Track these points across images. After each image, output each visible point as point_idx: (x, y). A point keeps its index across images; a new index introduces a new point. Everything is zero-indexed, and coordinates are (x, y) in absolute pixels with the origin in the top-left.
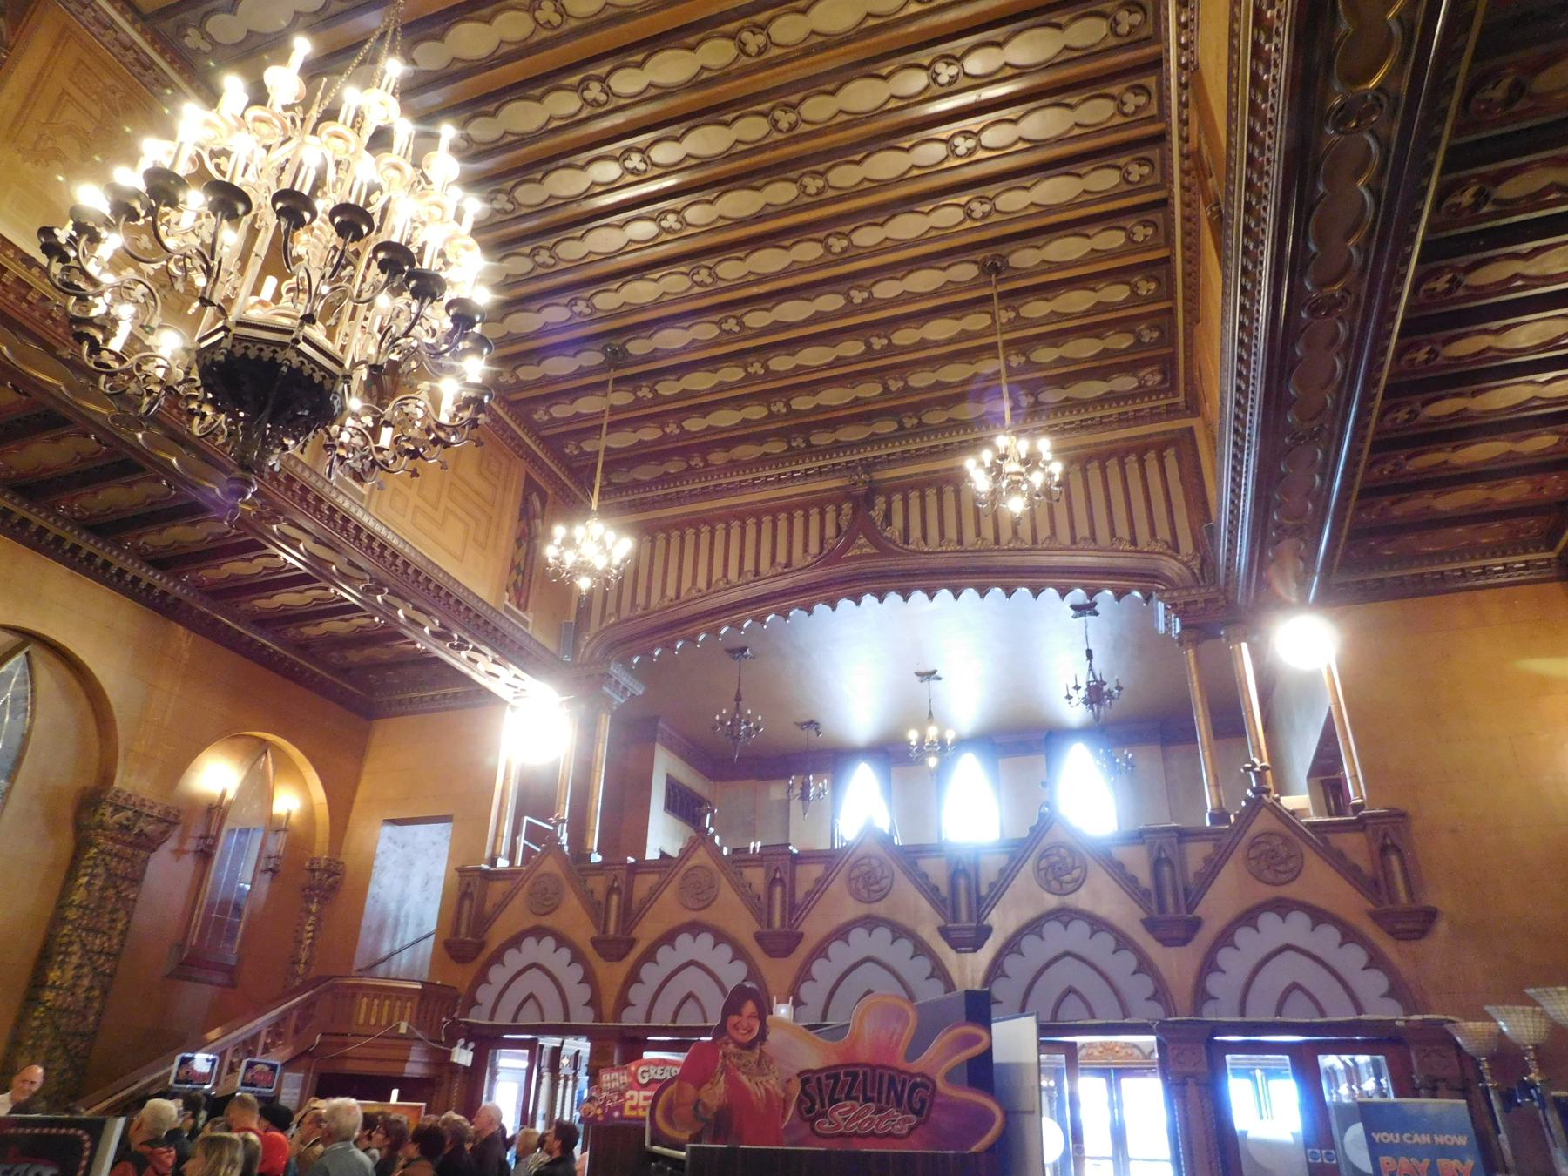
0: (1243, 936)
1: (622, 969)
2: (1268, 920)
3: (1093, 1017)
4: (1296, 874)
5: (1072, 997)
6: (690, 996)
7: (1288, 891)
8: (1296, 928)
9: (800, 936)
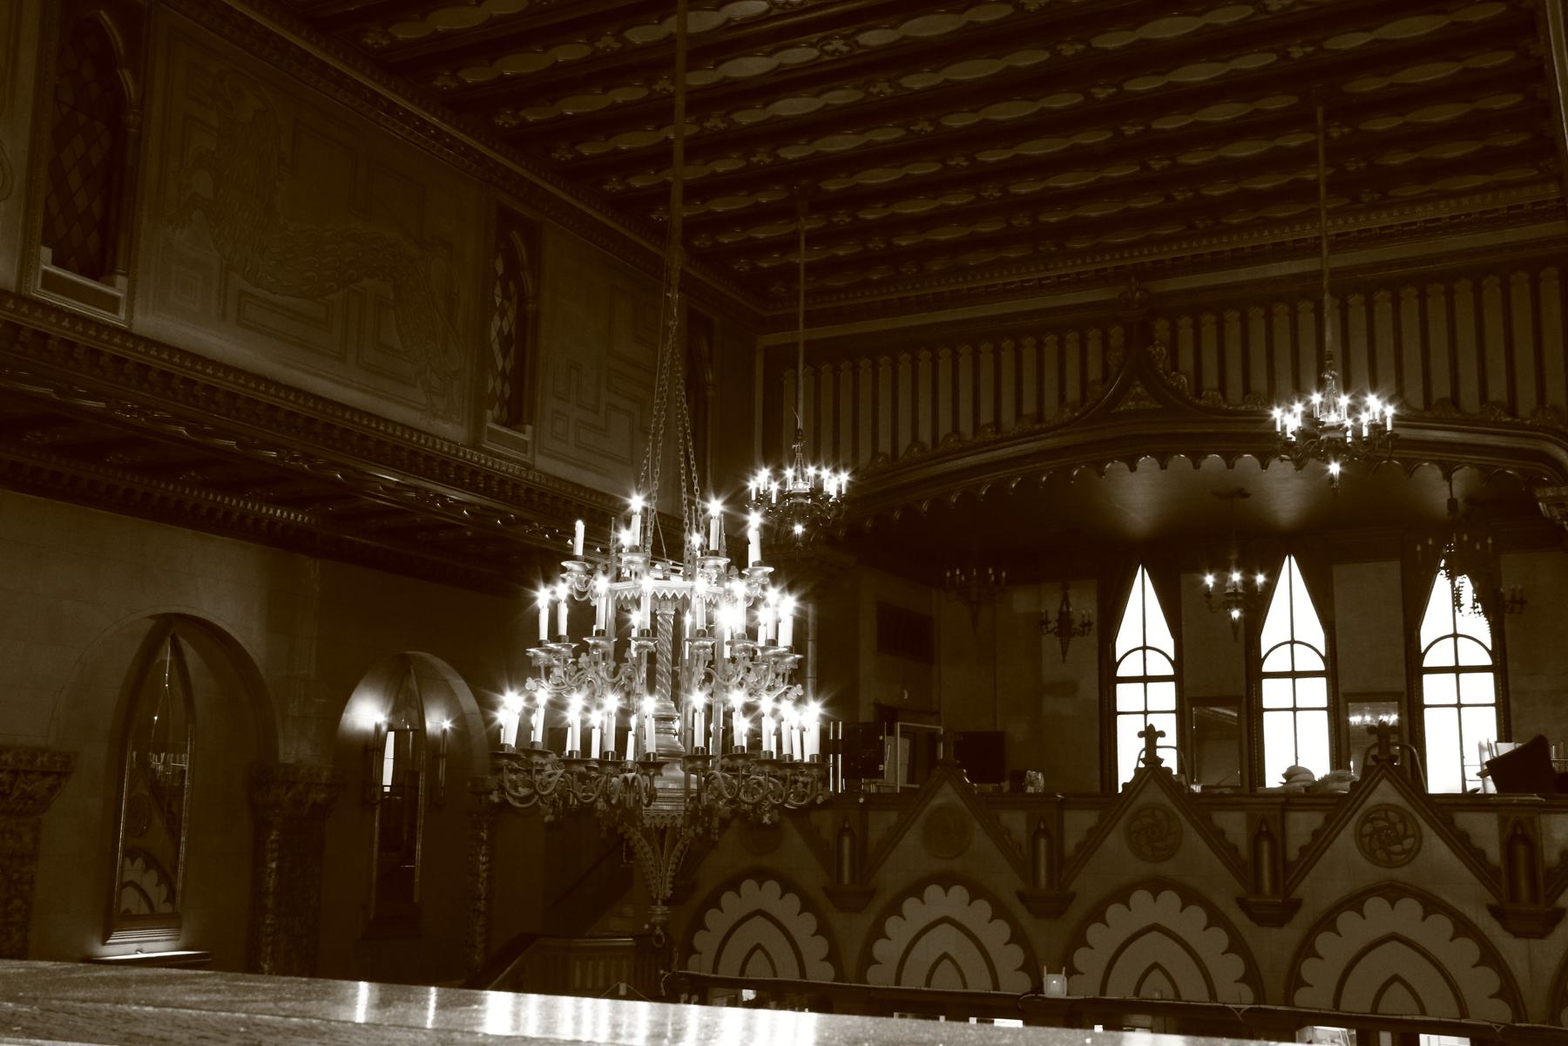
0: (1346, 920)
1: (1290, 935)
2: (1375, 905)
3: (775, 976)
4: (1411, 854)
5: (1397, 986)
6: (758, 947)
7: (1401, 874)
8: (1166, 908)
9: (1072, 897)
